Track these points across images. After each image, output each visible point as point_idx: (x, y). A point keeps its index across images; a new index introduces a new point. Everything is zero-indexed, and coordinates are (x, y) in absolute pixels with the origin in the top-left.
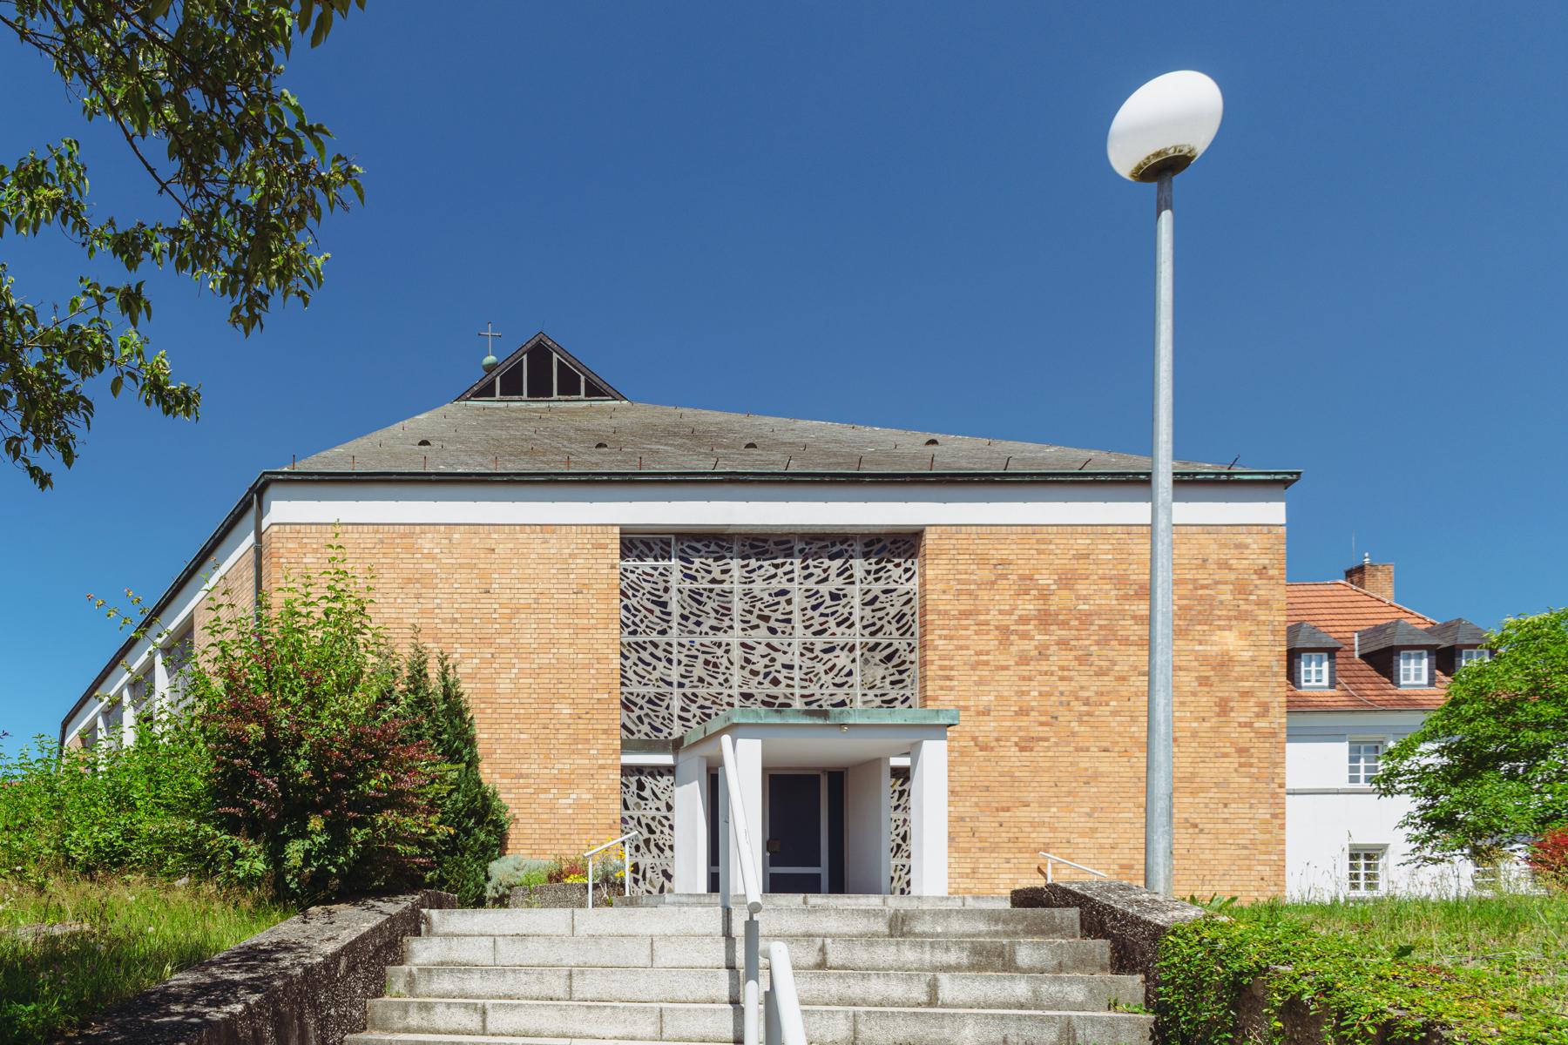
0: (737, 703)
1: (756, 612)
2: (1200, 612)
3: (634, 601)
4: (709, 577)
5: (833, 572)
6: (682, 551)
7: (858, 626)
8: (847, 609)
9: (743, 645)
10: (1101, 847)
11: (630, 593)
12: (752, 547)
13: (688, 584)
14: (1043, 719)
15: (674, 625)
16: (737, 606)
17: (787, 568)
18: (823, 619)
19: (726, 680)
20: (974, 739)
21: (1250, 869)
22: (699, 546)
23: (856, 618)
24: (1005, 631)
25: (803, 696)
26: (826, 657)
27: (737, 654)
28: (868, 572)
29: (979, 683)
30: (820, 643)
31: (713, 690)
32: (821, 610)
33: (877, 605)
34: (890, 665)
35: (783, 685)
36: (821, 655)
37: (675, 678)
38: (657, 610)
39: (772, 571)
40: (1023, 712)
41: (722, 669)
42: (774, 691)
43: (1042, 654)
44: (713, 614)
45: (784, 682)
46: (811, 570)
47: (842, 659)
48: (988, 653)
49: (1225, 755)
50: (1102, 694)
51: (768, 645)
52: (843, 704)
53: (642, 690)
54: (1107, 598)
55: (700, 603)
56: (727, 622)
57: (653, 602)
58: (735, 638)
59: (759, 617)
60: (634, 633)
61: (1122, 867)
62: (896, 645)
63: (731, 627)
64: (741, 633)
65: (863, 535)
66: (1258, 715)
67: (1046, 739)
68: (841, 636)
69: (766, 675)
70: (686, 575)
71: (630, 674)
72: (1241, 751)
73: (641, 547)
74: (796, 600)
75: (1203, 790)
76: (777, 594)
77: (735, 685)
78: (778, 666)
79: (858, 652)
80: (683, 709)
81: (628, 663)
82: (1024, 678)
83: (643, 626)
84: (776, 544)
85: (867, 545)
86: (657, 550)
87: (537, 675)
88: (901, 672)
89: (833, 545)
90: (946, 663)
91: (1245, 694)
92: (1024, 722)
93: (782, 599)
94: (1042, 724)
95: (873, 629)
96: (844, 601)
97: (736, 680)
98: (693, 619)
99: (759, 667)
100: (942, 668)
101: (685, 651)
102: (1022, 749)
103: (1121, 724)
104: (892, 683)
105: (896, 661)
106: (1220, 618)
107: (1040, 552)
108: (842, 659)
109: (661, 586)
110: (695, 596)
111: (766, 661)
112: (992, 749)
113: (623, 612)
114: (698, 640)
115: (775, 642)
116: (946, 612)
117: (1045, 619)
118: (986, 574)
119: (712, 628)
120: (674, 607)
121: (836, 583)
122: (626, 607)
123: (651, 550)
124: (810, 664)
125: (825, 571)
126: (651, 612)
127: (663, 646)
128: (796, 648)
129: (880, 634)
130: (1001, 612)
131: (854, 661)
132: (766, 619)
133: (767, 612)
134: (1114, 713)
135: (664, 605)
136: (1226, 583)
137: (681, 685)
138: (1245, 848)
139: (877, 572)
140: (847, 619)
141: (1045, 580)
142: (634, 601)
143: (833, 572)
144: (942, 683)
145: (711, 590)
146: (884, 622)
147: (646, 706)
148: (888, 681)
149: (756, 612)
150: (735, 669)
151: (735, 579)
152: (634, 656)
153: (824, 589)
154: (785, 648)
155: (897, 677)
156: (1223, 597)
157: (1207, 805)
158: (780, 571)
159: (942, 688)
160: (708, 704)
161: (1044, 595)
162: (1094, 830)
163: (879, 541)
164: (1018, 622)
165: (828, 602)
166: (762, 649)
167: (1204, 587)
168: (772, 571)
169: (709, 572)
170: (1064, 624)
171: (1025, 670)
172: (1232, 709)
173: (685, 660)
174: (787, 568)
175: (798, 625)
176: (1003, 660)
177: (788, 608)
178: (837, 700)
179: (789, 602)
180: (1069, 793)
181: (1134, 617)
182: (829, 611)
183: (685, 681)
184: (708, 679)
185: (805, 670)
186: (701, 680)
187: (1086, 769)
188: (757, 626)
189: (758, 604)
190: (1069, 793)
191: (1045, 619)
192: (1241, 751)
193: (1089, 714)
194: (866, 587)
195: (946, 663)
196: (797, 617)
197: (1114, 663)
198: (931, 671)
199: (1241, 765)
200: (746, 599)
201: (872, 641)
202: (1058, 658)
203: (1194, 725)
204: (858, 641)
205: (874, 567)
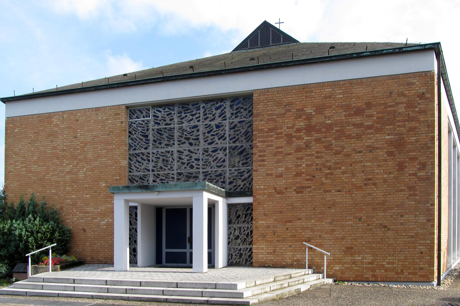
0: (176, 177)
1: (184, 136)
2: (388, 119)
3: (135, 136)
4: (165, 123)
5: (217, 115)
6: (154, 112)
7: (228, 139)
8: (223, 132)
9: (179, 151)
10: (337, 238)
11: (133, 133)
12: (183, 108)
13: (156, 127)
14: (308, 177)
15: (151, 145)
16: (176, 134)
17: (197, 115)
18: (212, 137)
19: (171, 167)
20: (275, 189)
21: (415, 248)
22: (161, 109)
23: (227, 135)
24: (289, 137)
25: (203, 172)
26: (213, 154)
27: (176, 155)
28: (232, 114)
29: (277, 162)
30: (211, 148)
31: (166, 172)
32: (212, 133)
33: (236, 129)
34: (242, 156)
35: (195, 168)
36: (211, 153)
37: (151, 168)
38: (144, 139)
39: (191, 117)
40: (298, 174)
41: (170, 163)
42: (191, 171)
43: (308, 146)
44: (166, 139)
45: (196, 166)
46: (208, 115)
47: (220, 155)
48: (281, 148)
49: (402, 191)
50: (337, 163)
51: (189, 151)
52: (221, 175)
53: (138, 174)
54: (341, 116)
55: (161, 134)
56: (172, 142)
57: (143, 136)
58: (175, 149)
59: (186, 138)
60: (135, 149)
61: (347, 248)
62: (245, 146)
63: (174, 144)
64: (178, 146)
65: (230, 98)
66: (419, 169)
67: (309, 187)
68: (220, 144)
69: (188, 164)
70: (156, 123)
71: (133, 167)
72: (411, 188)
73: (138, 112)
74: (201, 130)
75: (391, 209)
76: (193, 128)
77: (175, 170)
78: (193, 160)
79: (228, 151)
80: (154, 181)
81: (132, 163)
82: (299, 158)
83: (138, 146)
84: (193, 105)
85: (232, 102)
86: (144, 114)
87: (92, 170)
88: (247, 159)
89: (217, 103)
90: (262, 154)
91: (413, 159)
92: (298, 179)
93: (195, 130)
94: (307, 180)
95: (234, 140)
96: (222, 128)
97: (175, 167)
98: (158, 141)
99: (185, 161)
100: (260, 156)
101: (155, 156)
102: (298, 193)
103: (346, 178)
104: (243, 164)
105: (244, 154)
106: (399, 121)
107: (306, 97)
108: (220, 155)
109: (146, 128)
110: (159, 132)
111: (188, 158)
112: (283, 193)
113: (131, 141)
114: (160, 150)
115: (192, 148)
116: (262, 130)
117: (309, 129)
118: (281, 111)
119: (166, 145)
120: (151, 137)
121: (218, 120)
122: (132, 139)
123: (142, 113)
124: (207, 158)
125: (213, 115)
126: (141, 140)
127: (146, 154)
128: (201, 151)
129: (237, 142)
130: (288, 128)
131: (226, 155)
132: (188, 139)
133: (188, 136)
134: (343, 173)
135: (147, 136)
136: (402, 103)
137: (153, 171)
138: (412, 237)
139: (236, 113)
140: (223, 136)
141: (309, 110)
142: (135, 136)
143: (217, 115)
144: (260, 163)
145: (166, 128)
146: (239, 136)
147: (139, 180)
148: (241, 163)
149: (184, 136)
150: (175, 162)
151: (176, 123)
152: (134, 159)
153: (213, 123)
154: (196, 151)
155: (245, 161)
156: (400, 111)
157: (391, 216)
158: (194, 117)
159: (260, 166)
160: (164, 178)
161: (309, 117)
162: (333, 231)
163: (237, 99)
164: (296, 132)
165: (215, 129)
166: (186, 153)
167: (390, 106)
168: (191, 117)
169: (165, 121)
170: (319, 131)
171: (299, 155)
172: (406, 167)
173: (155, 160)
174: (197, 115)
175: (202, 141)
176: (288, 150)
177: (198, 134)
178: (218, 173)
179: (198, 131)
180: (321, 213)
181: (354, 125)
182: (215, 133)
183: (155, 169)
184: (164, 167)
185: (204, 161)
186: (161, 168)
187: (329, 201)
188: (184, 143)
189: (185, 133)
190: (321, 213)
191: (309, 129)
192: (411, 188)
193: (331, 174)
194: (231, 121)
195: (262, 154)
196: (201, 137)
197: (343, 148)
198: (255, 158)
199: (410, 195)
200: (180, 131)
201: (234, 145)
202: (315, 147)
203: (385, 176)
204: (227, 146)
205: (235, 111)
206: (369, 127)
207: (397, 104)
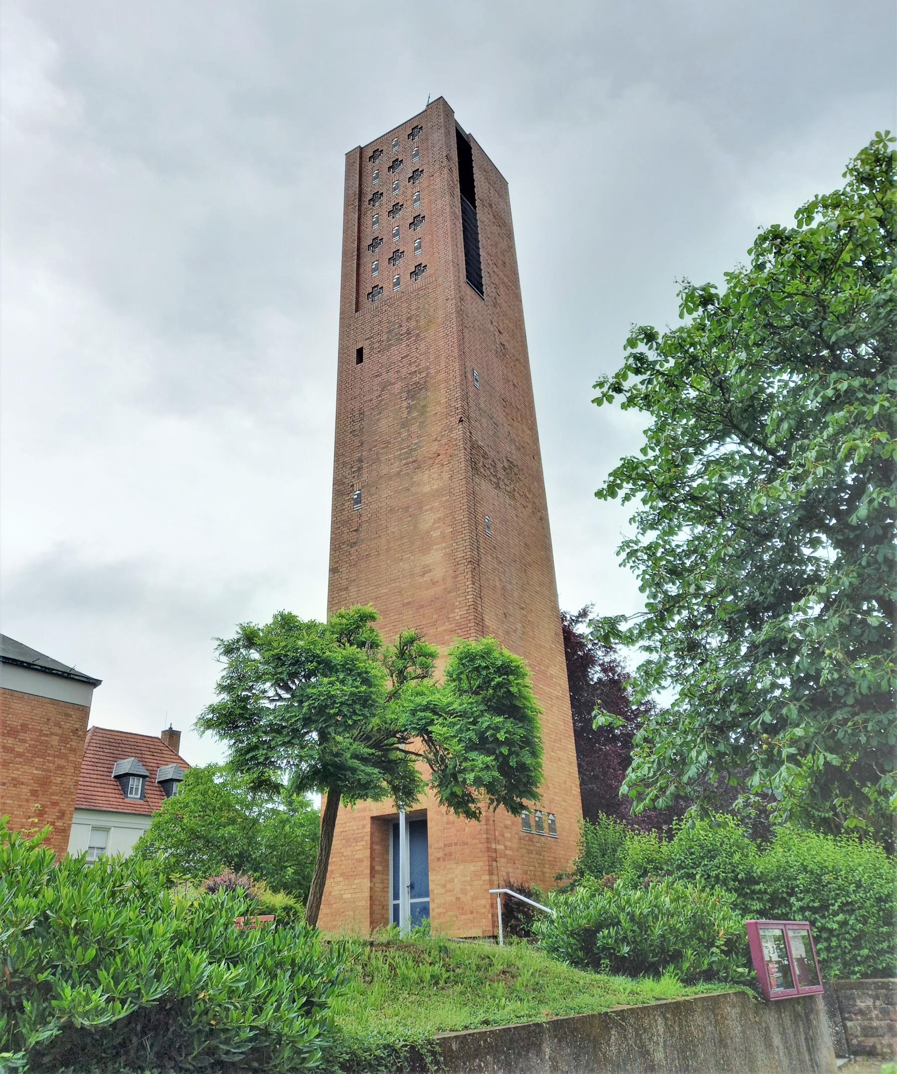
91: (55, 804)
206: (20, 755)
207: (52, 734)
